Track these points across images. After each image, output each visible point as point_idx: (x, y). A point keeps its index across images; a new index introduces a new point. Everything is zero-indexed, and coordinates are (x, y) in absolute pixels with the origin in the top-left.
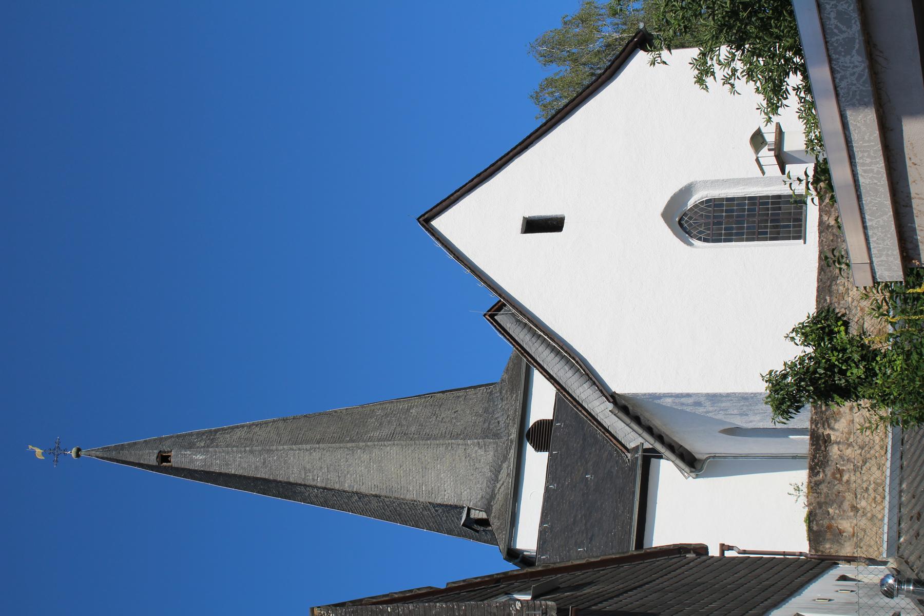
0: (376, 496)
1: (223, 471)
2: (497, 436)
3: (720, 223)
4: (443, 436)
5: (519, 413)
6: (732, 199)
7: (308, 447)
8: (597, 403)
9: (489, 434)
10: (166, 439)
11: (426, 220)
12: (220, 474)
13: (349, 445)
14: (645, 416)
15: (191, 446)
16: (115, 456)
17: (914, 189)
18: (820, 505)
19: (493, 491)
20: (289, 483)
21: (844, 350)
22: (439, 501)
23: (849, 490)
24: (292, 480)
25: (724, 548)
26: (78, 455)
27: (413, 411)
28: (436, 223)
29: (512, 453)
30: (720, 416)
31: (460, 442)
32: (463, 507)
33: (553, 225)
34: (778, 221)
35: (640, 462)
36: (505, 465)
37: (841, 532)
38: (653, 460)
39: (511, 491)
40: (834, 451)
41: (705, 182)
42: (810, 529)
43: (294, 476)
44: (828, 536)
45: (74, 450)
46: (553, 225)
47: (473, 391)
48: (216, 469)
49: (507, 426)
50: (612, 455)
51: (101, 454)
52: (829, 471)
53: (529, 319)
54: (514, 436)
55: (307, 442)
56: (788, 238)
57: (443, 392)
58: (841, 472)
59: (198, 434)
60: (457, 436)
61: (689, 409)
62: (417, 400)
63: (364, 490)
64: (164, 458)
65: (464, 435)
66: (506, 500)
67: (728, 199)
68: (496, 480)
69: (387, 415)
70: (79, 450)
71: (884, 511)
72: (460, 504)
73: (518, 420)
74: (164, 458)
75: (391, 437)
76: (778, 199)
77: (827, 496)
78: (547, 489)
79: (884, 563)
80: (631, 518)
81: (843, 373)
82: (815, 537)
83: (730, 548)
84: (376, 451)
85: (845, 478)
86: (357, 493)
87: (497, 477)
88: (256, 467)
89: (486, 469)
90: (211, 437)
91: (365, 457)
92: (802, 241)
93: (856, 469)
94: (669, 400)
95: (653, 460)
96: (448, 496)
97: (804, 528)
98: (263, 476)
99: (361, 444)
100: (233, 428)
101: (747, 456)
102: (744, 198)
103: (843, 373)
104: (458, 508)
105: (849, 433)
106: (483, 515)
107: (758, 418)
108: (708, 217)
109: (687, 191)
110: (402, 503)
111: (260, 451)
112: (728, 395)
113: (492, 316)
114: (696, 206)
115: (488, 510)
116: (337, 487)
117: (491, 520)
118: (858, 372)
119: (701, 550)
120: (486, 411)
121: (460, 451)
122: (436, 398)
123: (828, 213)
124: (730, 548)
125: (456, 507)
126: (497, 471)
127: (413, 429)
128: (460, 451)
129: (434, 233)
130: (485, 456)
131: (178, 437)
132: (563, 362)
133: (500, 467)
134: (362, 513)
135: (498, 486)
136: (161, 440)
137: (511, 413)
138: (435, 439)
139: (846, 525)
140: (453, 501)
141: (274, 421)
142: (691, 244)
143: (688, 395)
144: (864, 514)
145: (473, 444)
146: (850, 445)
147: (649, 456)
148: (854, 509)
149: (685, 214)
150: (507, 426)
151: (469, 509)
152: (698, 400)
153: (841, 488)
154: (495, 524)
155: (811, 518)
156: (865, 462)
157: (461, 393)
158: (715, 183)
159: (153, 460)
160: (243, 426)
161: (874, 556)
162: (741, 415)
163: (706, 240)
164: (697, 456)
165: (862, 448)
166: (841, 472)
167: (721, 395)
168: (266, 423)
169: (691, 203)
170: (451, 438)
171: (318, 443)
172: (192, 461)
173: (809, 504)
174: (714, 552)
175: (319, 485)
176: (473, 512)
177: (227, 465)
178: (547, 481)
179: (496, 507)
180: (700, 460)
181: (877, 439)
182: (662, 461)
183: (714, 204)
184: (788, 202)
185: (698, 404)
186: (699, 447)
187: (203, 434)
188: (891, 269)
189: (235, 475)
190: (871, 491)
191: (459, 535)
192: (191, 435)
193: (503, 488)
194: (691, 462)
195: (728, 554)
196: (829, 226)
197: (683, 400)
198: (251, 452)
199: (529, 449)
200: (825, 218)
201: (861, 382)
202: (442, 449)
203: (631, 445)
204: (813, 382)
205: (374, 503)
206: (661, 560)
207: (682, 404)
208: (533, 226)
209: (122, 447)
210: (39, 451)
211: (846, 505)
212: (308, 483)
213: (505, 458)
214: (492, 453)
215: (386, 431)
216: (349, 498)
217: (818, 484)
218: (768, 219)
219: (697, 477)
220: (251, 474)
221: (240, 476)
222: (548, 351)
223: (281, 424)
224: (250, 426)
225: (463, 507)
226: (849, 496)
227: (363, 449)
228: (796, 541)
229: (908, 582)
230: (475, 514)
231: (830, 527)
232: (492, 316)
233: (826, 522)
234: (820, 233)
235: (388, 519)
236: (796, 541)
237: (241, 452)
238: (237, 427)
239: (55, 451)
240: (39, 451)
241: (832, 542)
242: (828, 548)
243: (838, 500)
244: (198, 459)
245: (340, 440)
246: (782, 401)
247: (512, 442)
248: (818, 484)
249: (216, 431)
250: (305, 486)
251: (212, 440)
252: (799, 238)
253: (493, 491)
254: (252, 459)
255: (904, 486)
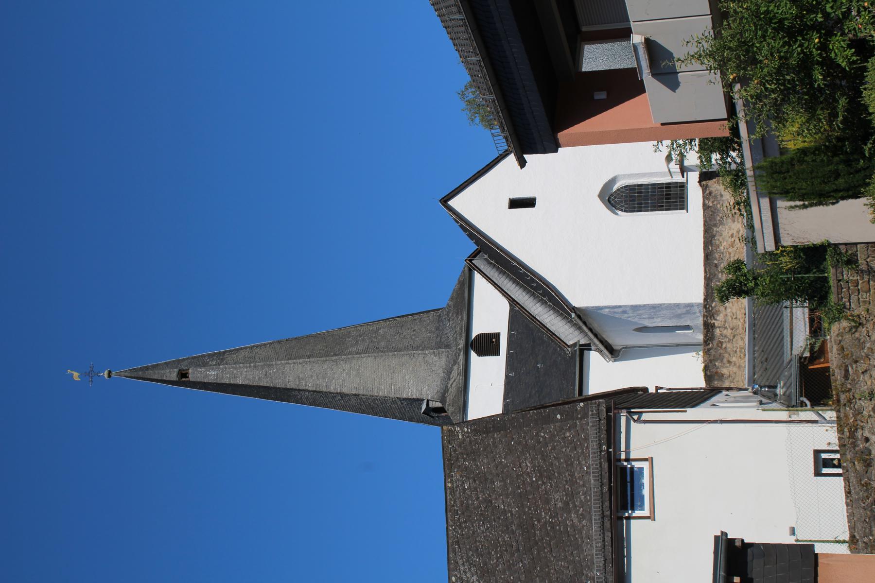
0: (355, 395)
1: (232, 382)
2: (448, 346)
3: (634, 200)
4: (406, 349)
5: (464, 330)
6: (641, 185)
7: (301, 361)
8: (546, 316)
9: (441, 345)
10: (183, 360)
11: (445, 201)
12: (230, 385)
13: (334, 358)
14: (589, 321)
15: (204, 365)
16: (141, 375)
17: (780, 221)
18: (711, 361)
19: (446, 386)
20: (287, 389)
21: (745, 276)
22: (405, 396)
23: (726, 352)
24: (288, 386)
25: (657, 388)
26: (109, 376)
27: (381, 331)
28: (451, 203)
29: (461, 358)
30: (636, 320)
31: (420, 352)
32: (423, 400)
33: (529, 203)
34: (670, 199)
35: (578, 353)
36: (455, 367)
37: (723, 375)
38: (586, 352)
39: (461, 385)
40: (717, 332)
41: (625, 175)
42: (706, 375)
43: (290, 384)
44: (716, 377)
45: (106, 372)
46: (529, 203)
47: (425, 315)
48: (227, 381)
49: (455, 339)
50: (556, 350)
51: (126, 374)
52: (715, 343)
53: (518, 263)
54: (462, 345)
55: (300, 358)
56: (676, 209)
57: (403, 316)
58: (721, 343)
59: (209, 355)
60: (417, 348)
61: (617, 316)
62: (383, 324)
63: (346, 391)
64: (183, 375)
65: (422, 347)
66: (458, 391)
67: (638, 185)
68: (449, 378)
69: (361, 335)
70: (110, 372)
71: (745, 363)
72: (422, 397)
73: (464, 334)
74: (183, 375)
75: (366, 351)
76: (668, 186)
77: (714, 356)
78: (507, 377)
79: (746, 390)
80: (574, 389)
81: (745, 285)
82: (708, 378)
83: (661, 388)
84: (355, 362)
85: (724, 346)
86: (340, 393)
87: (449, 376)
88: (259, 378)
89: (440, 371)
90: (220, 358)
91: (347, 366)
92: (685, 211)
93: (729, 341)
94: (607, 310)
95: (586, 352)
96: (411, 392)
97: (702, 375)
98: (265, 384)
99: (343, 357)
100: (238, 350)
101: (647, 346)
102: (648, 185)
103: (745, 285)
104: (419, 401)
105: (725, 322)
106: (439, 405)
107: (659, 320)
108: (626, 197)
109: (613, 181)
110: (375, 399)
111: (262, 366)
112: (644, 306)
113: (471, 261)
114: (618, 190)
115: (443, 400)
116: (324, 390)
117: (446, 408)
118: (752, 284)
119: (645, 390)
120: (437, 329)
121: (420, 358)
122: (399, 321)
123: (708, 199)
124: (661, 388)
125: (418, 400)
126: (448, 372)
127: (383, 344)
128: (420, 358)
129: (450, 209)
130: (438, 361)
131: (193, 358)
132: (521, 290)
133: (452, 369)
134: (343, 408)
135: (451, 382)
136: (179, 361)
137: (458, 329)
138: (400, 351)
139: (725, 371)
140: (416, 395)
141: (271, 343)
142: (617, 214)
143: (620, 307)
144: (735, 364)
145: (430, 353)
146: (726, 328)
147: (585, 348)
148: (729, 362)
149: (612, 195)
150: (455, 339)
151: (428, 401)
152: (624, 309)
153: (722, 352)
154: (450, 410)
155: (706, 369)
156: (734, 337)
157: (417, 317)
158: (630, 176)
159: (173, 376)
160: (246, 348)
161: (740, 387)
162: (649, 318)
163: (625, 211)
164: (615, 348)
165: (732, 329)
166: (721, 343)
167: (640, 306)
168: (265, 345)
169: (615, 188)
170: (413, 349)
171: (309, 357)
172: (206, 376)
173: (705, 361)
174: (652, 390)
175: (310, 389)
176: (431, 403)
177: (236, 377)
178: (507, 371)
179: (449, 398)
180: (616, 351)
181: (740, 324)
182: (591, 352)
183: (630, 188)
184: (676, 187)
185: (624, 312)
186: (617, 342)
187: (214, 355)
188: (771, 246)
189: (242, 385)
190: (738, 353)
191: (418, 421)
192: (204, 356)
193: (455, 384)
194: (613, 352)
195: (660, 391)
196: (709, 207)
197: (616, 310)
198: (255, 367)
199: (473, 354)
200: (707, 202)
201: (753, 289)
202: (406, 358)
203: (570, 343)
204: (734, 289)
205: (353, 401)
206: (625, 396)
207: (615, 312)
208: (515, 204)
209: (147, 368)
210: (76, 375)
211: (725, 360)
212: (301, 388)
213: (455, 362)
214: (444, 359)
215: (361, 347)
216: (334, 397)
217: (709, 350)
218: (668, 197)
219: (615, 361)
220: (255, 383)
221: (253, 387)
222: (511, 283)
223: (276, 345)
224: (252, 348)
225: (423, 400)
226: (726, 355)
227: (345, 361)
228: (700, 383)
229: (765, 386)
230: (433, 404)
231: (717, 373)
232: (471, 261)
233: (714, 370)
234: (704, 210)
235: (363, 412)
236: (700, 383)
237: (247, 367)
238: (241, 349)
239: (90, 374)
240: (76, 375)
241: (718, 380)
242: (716, 384)
243: (720, 358)
244: (211, 375)
245: (327, 355)
246: (722, 297)
247: (460, 350)
248: (709, 350)
249: (224, 353)
250: (299, 390)
251: (222, 360)
252: (683, 209)
253: (446, 386)
254: (256, 372)
255: (756, 348)
